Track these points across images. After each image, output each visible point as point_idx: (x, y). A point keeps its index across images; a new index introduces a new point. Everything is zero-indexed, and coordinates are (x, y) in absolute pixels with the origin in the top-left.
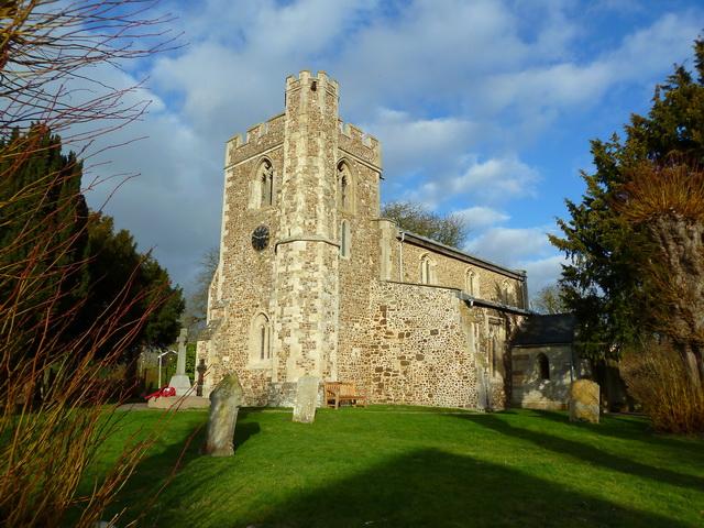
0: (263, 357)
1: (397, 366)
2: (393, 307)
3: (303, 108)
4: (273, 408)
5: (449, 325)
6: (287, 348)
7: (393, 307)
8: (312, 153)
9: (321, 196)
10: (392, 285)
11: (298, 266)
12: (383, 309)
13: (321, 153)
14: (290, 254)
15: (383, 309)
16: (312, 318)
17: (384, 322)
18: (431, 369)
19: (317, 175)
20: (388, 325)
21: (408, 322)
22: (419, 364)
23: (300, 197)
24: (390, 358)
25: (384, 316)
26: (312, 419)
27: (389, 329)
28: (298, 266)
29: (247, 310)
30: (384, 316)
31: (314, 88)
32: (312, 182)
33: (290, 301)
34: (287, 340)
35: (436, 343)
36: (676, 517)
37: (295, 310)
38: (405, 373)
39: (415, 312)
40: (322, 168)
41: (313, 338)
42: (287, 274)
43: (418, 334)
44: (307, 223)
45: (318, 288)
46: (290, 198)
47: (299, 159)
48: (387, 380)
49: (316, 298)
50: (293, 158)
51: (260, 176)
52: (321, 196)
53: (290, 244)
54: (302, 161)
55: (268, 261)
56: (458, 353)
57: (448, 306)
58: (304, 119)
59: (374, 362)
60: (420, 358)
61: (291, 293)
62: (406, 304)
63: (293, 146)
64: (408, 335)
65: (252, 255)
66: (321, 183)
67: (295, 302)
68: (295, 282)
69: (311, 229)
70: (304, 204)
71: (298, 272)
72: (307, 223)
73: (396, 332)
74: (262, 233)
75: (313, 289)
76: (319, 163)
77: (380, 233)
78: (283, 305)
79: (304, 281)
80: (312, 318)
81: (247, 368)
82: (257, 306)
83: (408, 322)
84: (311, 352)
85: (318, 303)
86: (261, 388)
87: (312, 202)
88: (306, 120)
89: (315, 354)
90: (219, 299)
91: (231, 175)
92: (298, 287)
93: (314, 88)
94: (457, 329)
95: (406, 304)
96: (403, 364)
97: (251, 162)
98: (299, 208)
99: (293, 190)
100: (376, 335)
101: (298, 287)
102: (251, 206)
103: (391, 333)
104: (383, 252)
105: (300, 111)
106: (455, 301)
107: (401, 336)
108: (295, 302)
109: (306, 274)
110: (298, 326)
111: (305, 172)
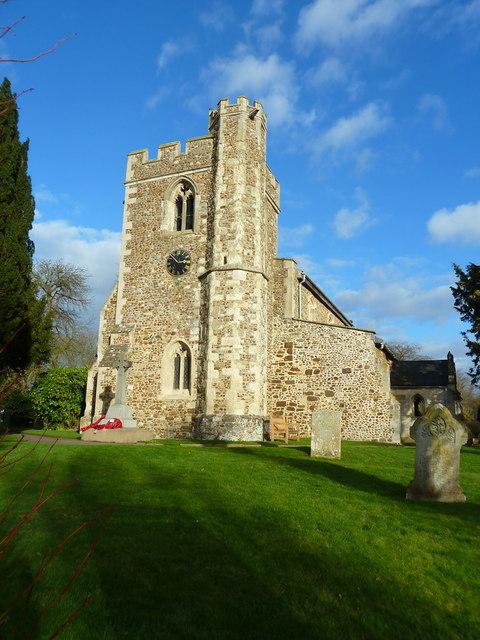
0: (177, 386)
1: (303, 401)
2: (300, 344)
3: (242, 135)
4: (236, 443)
5: (364, 365)
6: (227, 381)
7: (300, 344)
8: (250, 182)
9: (258, 228)
10: (299, 324)
11: (238, 296)
12: (289, 346)
13: (258, 184)
14: (229, 283)
15: (289, 346)
16: (252, 350)
17: (289, 358)
18: (342, 405)
19: (254, 206)
20: (294, 361)
21: (317, 360)
22: (329, 399)
23: (239, 225)
24: (297, 393)
25: (290, 352)
26: (339, 455)
27: (295, 365)
28: (238, 296)
29: (158, 337)
30: (290, 352)
31: (252, 118)
32: (250, 212)
33: (230, 331)
34: (226, 372)
35: (348, 381)
36: (433, 516)
37: (236, 341)
38: (312, 408)
39: (324, 351)
40: (258, 200)
41: (252, 370)
42: (226, 304)
43: (326, 373)
44: (245, 254)
45: (257, 320)
46: (227, 225)
47: (238, 187)
48: (291, 414)
49: (255, 330)
50: (230, 185)
51: (174, 197)
52: (258, 228)
53: (229, 273)
54: (241, 189)
55: (188, 287)
56: (373, 391)
57: (362, 347)
58: (242, 146)
59: (276, 397)
60: (329, 394)
61: (230, 323)
62: (315, 343)
63: (229, 171)
64: (317, 372)
65: (167, 280)
66: (258, 214)
67: (236, 332)
68: (235, 311)
69: (249, 259)
70: (243, 233)
71: (239, 302)
72: (245, 254)
73: (303, 369)
74: (181, 257)
75: (252, 321)
76: (256, 193)
77: (284, 272)
78: (221, 334)
79: (245, 312)
80: (252, 350)
81: (160, 398)
82: (173, 333)
83: (317, 360)
84: (251, 385)
85: (256, 335)
86: (178, 419)
87: (250, 233)
88: (244, 148)
89: (253, 387)
90: (118, 321)
91: (134, 190)
92: (239, 318)
93: (252, 118)
94: (373, 369)
95: (315, 343)
96: (310, 399)
97: (164, 180)
98: (239, 236)
99: (231, 217)
100: (278, 371)
101: (239, 318)
102: (164, 227)
103: (297, 369)
104: (289, 291)
105: (238, 138)
106: (370, 344)
107: (308, 372)
108: (236, 332)
109: (246, 305)
110: (238, 357)
111: (244, 200)
